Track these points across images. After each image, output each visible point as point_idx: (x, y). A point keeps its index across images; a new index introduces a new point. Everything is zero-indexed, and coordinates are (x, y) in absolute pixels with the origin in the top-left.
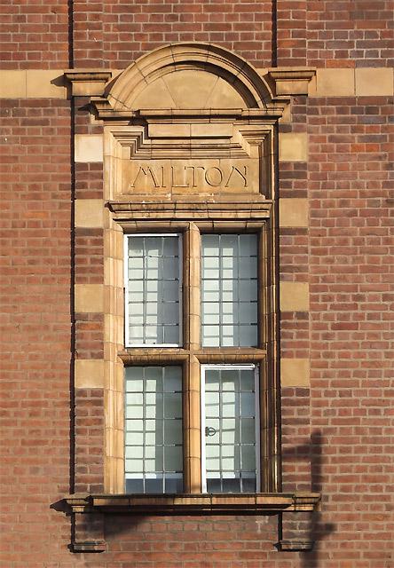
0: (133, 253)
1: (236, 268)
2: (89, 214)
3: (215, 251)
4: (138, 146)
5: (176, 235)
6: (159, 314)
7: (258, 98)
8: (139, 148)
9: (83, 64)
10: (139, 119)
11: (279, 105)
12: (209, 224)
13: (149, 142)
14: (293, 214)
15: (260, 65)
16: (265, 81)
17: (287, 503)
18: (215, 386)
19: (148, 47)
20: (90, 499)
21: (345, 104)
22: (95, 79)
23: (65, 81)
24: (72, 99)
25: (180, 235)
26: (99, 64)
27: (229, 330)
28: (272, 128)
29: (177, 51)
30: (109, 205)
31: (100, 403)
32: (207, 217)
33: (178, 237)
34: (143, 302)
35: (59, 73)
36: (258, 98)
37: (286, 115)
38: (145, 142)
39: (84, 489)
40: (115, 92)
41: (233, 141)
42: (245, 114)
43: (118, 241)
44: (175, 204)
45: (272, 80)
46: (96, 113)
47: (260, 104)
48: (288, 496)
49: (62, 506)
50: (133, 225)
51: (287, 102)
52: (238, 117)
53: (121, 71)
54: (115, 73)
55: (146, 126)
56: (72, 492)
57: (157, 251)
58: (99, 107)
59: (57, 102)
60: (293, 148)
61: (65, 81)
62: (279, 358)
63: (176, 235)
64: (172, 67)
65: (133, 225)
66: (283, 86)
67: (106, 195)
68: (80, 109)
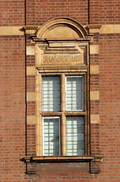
0: (68, 82)
1: (53, 87)
2: (30, 70)
3: (46, 82)
4: (46, 49)
5: (82, 77)
6: (77, 101)
7: (83, 35)
8: (46, 50)
9: (92, 23)
10: (46, 41)
11: (89, 37)
12: (44, 74)
13: (49, 48)
14: (94, 69)
15: (85, 24)
16: (85, 29)
17: (92, 159)
18: (47, 123)
19: (50, 19)
20: (32, 158)
21: (110, 35)
22: (28, 29)
23: (23, 30)
24: (25, 35)
25: (83, 77)
26: (33, 24)
27: (52, 106)
28: (88, 44)
29: (57, 20)
30: (37, 68)
31: (35, 129)
32: (67, 71)
33: (82, 77)
34: (71, 97)
35: (22, 27)
36: (83, 35)
37: (92, 39)
38: (48, 48)
39: (30, 155)
40: (39, 33)
41: (75, 48)
42: (79, 39)
43: (39, 78)
44: (44, 68)
45: (88, 29)
46: (33, 39)
47: (84, 36)
48: (93, 156)
49: (23, 160)
50: (68, 74)
51: (92, 35)
52: (77, 41)
53: (41, 26)
54: (39, 27)
55: (48, 43)
56: (26, 156)
57: (52, 81)
58: (33, 37)
59: (22, 36)
60: (94, 50)
61: (23, 30)
62: (90, 115)
63: (82, 77)
64: (57, 25)
65: (68, 74)
66: (92, 31)
67: (36, 65)
68: (28, 38)
